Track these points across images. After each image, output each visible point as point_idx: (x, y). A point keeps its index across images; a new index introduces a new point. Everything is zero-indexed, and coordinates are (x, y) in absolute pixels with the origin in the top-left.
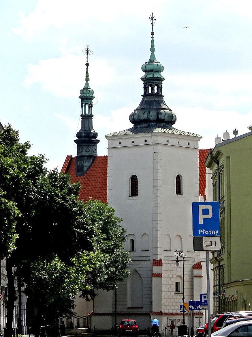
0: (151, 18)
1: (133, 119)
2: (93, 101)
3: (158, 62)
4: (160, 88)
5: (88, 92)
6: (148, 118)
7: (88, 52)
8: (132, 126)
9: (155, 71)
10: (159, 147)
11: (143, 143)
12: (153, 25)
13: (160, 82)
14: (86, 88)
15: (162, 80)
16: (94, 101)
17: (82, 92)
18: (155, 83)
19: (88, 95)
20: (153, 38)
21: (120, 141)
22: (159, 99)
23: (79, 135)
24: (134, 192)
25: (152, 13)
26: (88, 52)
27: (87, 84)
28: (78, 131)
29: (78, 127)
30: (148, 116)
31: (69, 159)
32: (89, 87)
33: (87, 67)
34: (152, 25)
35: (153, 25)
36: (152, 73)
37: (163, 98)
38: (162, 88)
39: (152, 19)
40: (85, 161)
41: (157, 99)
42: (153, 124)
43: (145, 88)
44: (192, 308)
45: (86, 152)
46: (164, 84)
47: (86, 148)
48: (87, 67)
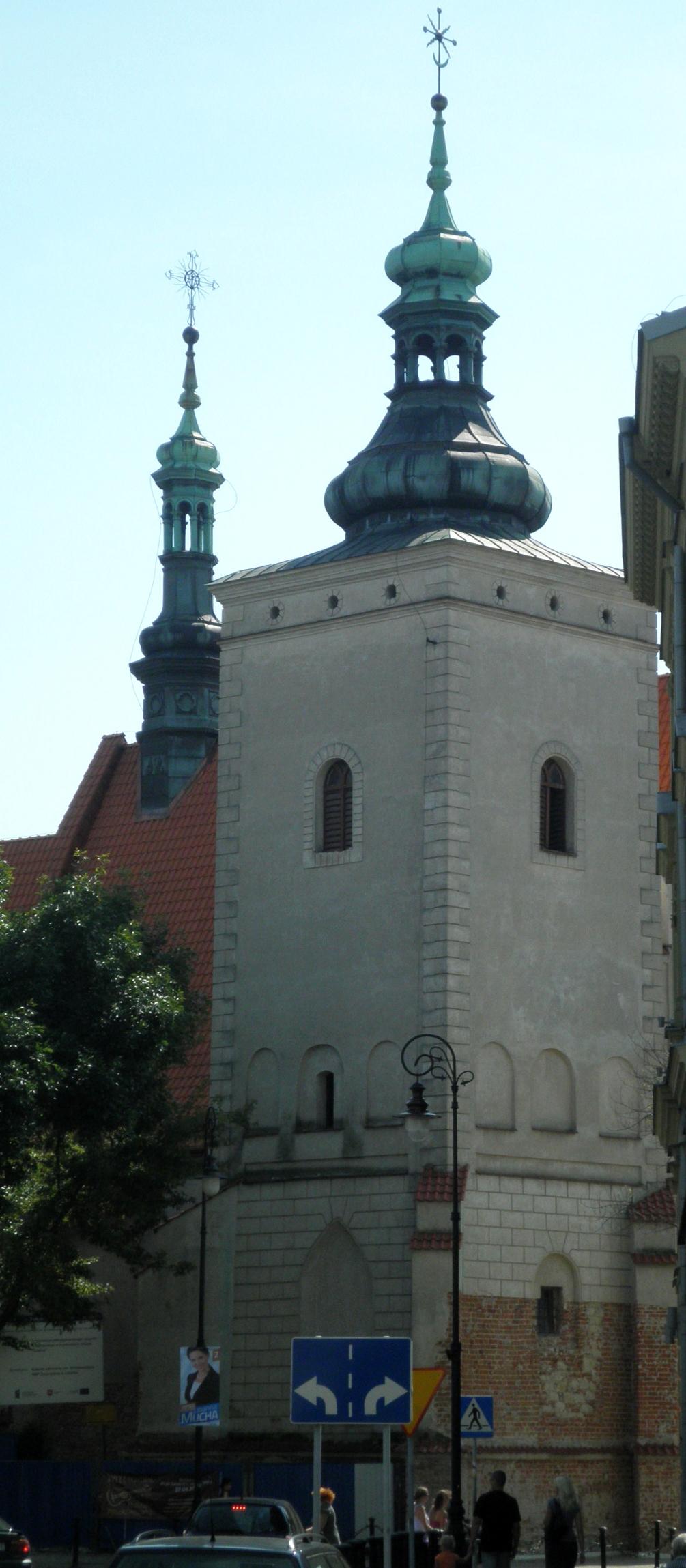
0: (430, 28)
1: (345, 501)
2: (216, 494)
3: (464, 234)
4: (473, 360)
5: (191, 451)
6: (407, 486)
7: (192, 280)
8: (336, 535)
9: (446, 274)
10: (453, 614)
11: (380, 601)
12: (442, 62)
13: (473, 325)
14: (185, 437)
15: (484, 317)
16: (221, 499)
17: (166, 452)
18: (448, 327)
19: (191, 465)
20: (439, 123)
21: (276, 601)
22: (464, 406)
23: (149, 639)
24: (335, 832)
25: (439, 11)
26: (192, 280)
27: (189, 422)
28: (149, 624)
29: (147, 602)
30: (405, 477)
31: (113, 749)
32: (195, 434)
33: (191, 348)
34: (438, 63)
35: (442, 62)
36: (434, 282)
37: (489, 404)
38: (483, 358)
39: (439, 37)
40: (173, 752)
41: (457, 406)
42: (432, 516)
43: (404, 360)
44: (321, 1402)
45: (179, 712)
46: (492, 341)
47: (178, 696)
48: (191, 348)
